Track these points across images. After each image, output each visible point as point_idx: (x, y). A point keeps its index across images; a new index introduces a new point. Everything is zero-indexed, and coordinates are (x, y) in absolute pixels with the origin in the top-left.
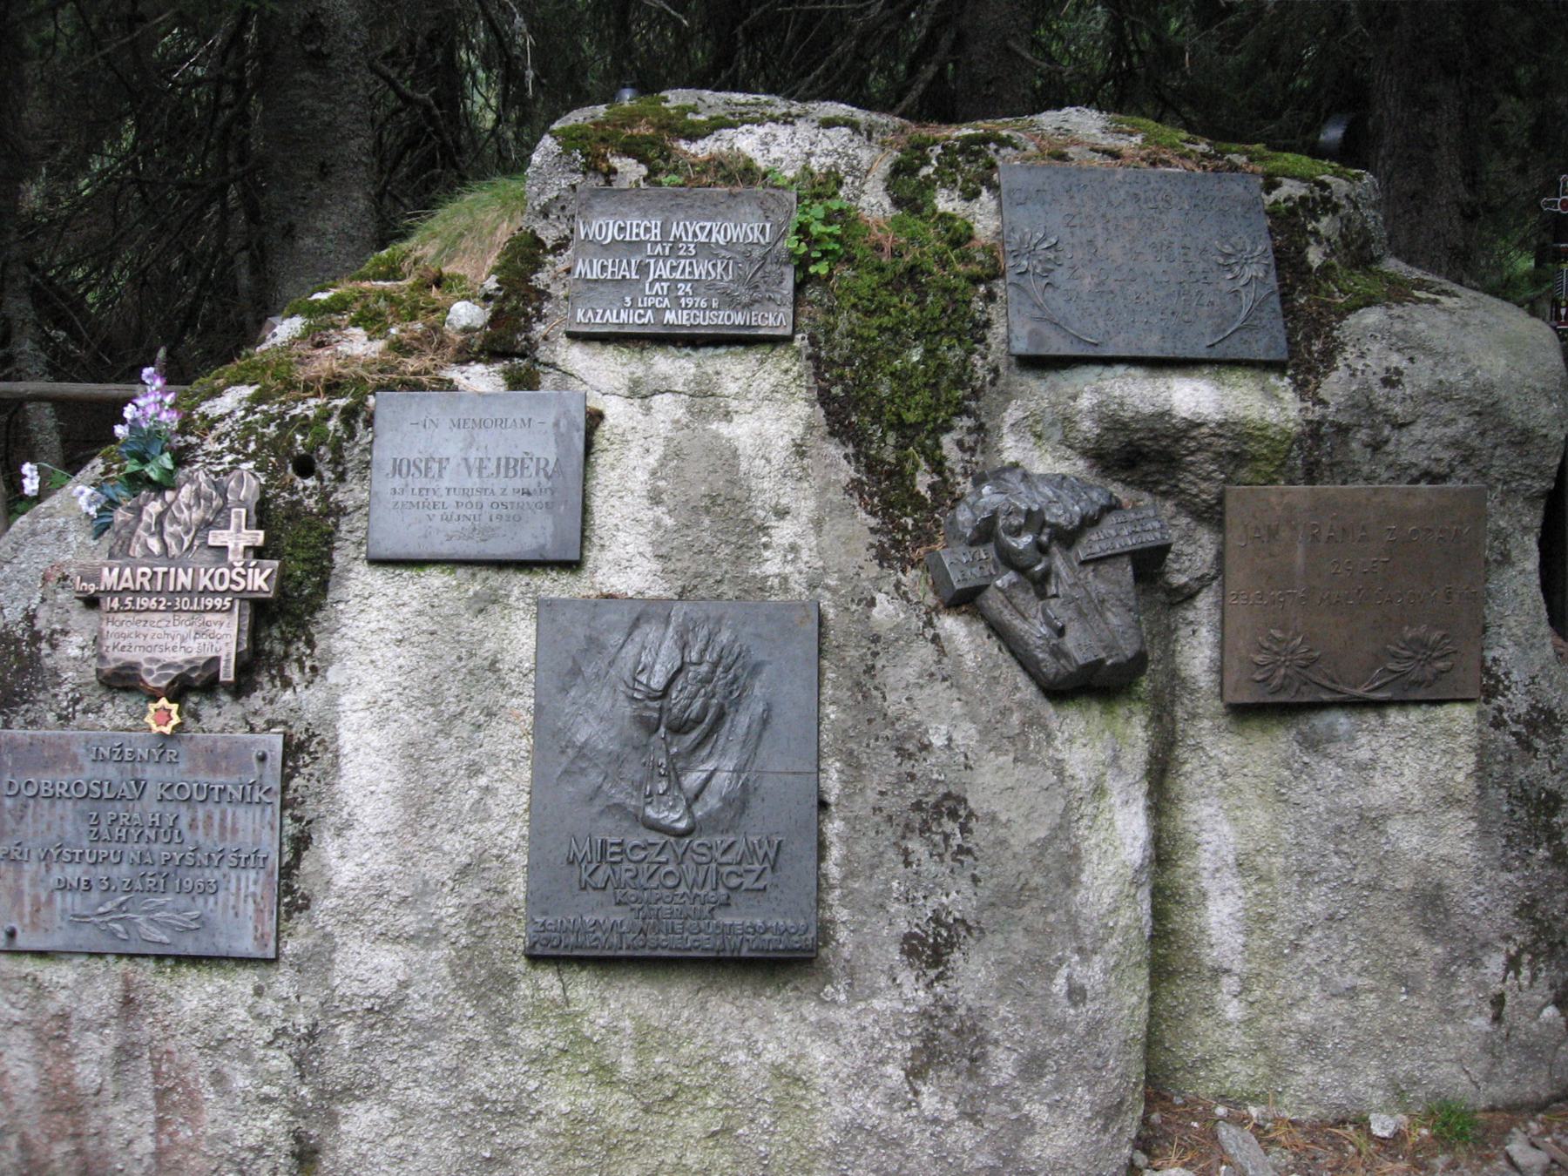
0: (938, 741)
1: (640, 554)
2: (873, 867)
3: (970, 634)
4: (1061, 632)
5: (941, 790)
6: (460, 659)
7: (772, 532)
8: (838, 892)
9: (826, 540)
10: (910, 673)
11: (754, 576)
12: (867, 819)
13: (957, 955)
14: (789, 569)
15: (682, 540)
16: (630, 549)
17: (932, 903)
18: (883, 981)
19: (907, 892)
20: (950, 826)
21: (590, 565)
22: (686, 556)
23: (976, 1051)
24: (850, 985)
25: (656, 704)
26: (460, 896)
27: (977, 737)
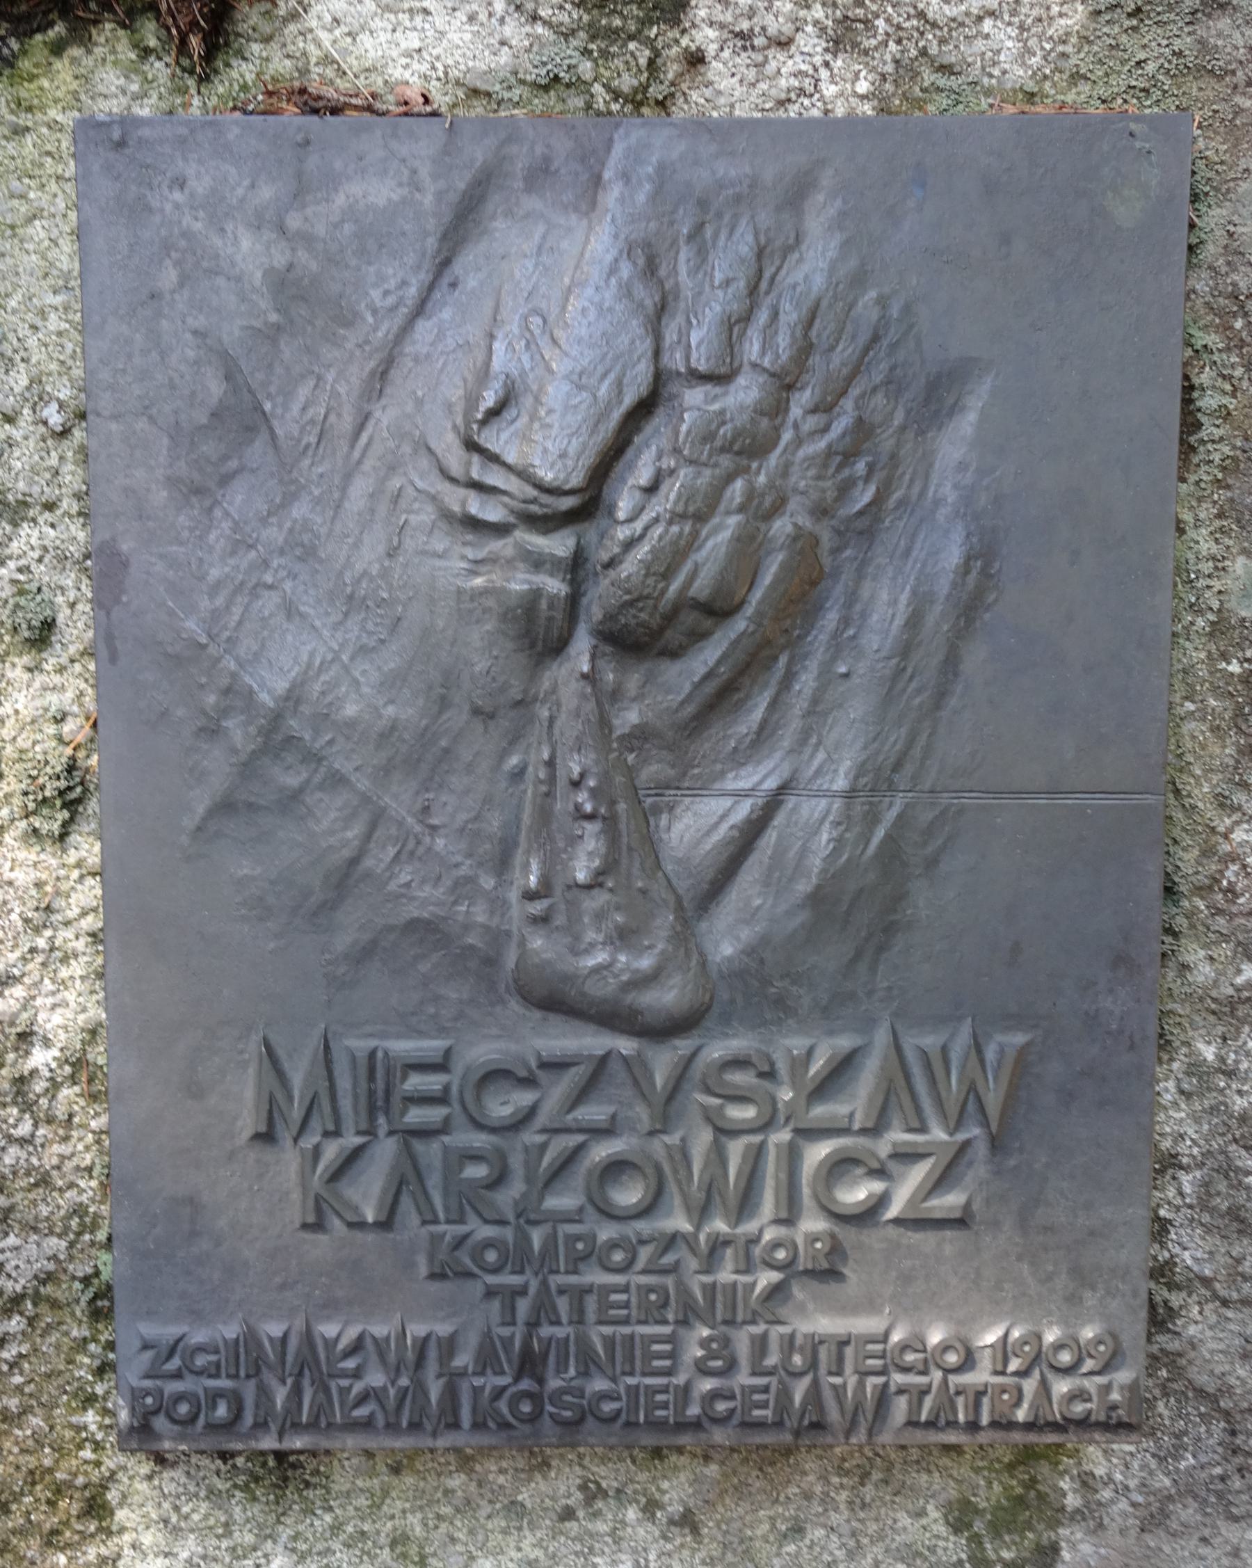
25: (559, 545)
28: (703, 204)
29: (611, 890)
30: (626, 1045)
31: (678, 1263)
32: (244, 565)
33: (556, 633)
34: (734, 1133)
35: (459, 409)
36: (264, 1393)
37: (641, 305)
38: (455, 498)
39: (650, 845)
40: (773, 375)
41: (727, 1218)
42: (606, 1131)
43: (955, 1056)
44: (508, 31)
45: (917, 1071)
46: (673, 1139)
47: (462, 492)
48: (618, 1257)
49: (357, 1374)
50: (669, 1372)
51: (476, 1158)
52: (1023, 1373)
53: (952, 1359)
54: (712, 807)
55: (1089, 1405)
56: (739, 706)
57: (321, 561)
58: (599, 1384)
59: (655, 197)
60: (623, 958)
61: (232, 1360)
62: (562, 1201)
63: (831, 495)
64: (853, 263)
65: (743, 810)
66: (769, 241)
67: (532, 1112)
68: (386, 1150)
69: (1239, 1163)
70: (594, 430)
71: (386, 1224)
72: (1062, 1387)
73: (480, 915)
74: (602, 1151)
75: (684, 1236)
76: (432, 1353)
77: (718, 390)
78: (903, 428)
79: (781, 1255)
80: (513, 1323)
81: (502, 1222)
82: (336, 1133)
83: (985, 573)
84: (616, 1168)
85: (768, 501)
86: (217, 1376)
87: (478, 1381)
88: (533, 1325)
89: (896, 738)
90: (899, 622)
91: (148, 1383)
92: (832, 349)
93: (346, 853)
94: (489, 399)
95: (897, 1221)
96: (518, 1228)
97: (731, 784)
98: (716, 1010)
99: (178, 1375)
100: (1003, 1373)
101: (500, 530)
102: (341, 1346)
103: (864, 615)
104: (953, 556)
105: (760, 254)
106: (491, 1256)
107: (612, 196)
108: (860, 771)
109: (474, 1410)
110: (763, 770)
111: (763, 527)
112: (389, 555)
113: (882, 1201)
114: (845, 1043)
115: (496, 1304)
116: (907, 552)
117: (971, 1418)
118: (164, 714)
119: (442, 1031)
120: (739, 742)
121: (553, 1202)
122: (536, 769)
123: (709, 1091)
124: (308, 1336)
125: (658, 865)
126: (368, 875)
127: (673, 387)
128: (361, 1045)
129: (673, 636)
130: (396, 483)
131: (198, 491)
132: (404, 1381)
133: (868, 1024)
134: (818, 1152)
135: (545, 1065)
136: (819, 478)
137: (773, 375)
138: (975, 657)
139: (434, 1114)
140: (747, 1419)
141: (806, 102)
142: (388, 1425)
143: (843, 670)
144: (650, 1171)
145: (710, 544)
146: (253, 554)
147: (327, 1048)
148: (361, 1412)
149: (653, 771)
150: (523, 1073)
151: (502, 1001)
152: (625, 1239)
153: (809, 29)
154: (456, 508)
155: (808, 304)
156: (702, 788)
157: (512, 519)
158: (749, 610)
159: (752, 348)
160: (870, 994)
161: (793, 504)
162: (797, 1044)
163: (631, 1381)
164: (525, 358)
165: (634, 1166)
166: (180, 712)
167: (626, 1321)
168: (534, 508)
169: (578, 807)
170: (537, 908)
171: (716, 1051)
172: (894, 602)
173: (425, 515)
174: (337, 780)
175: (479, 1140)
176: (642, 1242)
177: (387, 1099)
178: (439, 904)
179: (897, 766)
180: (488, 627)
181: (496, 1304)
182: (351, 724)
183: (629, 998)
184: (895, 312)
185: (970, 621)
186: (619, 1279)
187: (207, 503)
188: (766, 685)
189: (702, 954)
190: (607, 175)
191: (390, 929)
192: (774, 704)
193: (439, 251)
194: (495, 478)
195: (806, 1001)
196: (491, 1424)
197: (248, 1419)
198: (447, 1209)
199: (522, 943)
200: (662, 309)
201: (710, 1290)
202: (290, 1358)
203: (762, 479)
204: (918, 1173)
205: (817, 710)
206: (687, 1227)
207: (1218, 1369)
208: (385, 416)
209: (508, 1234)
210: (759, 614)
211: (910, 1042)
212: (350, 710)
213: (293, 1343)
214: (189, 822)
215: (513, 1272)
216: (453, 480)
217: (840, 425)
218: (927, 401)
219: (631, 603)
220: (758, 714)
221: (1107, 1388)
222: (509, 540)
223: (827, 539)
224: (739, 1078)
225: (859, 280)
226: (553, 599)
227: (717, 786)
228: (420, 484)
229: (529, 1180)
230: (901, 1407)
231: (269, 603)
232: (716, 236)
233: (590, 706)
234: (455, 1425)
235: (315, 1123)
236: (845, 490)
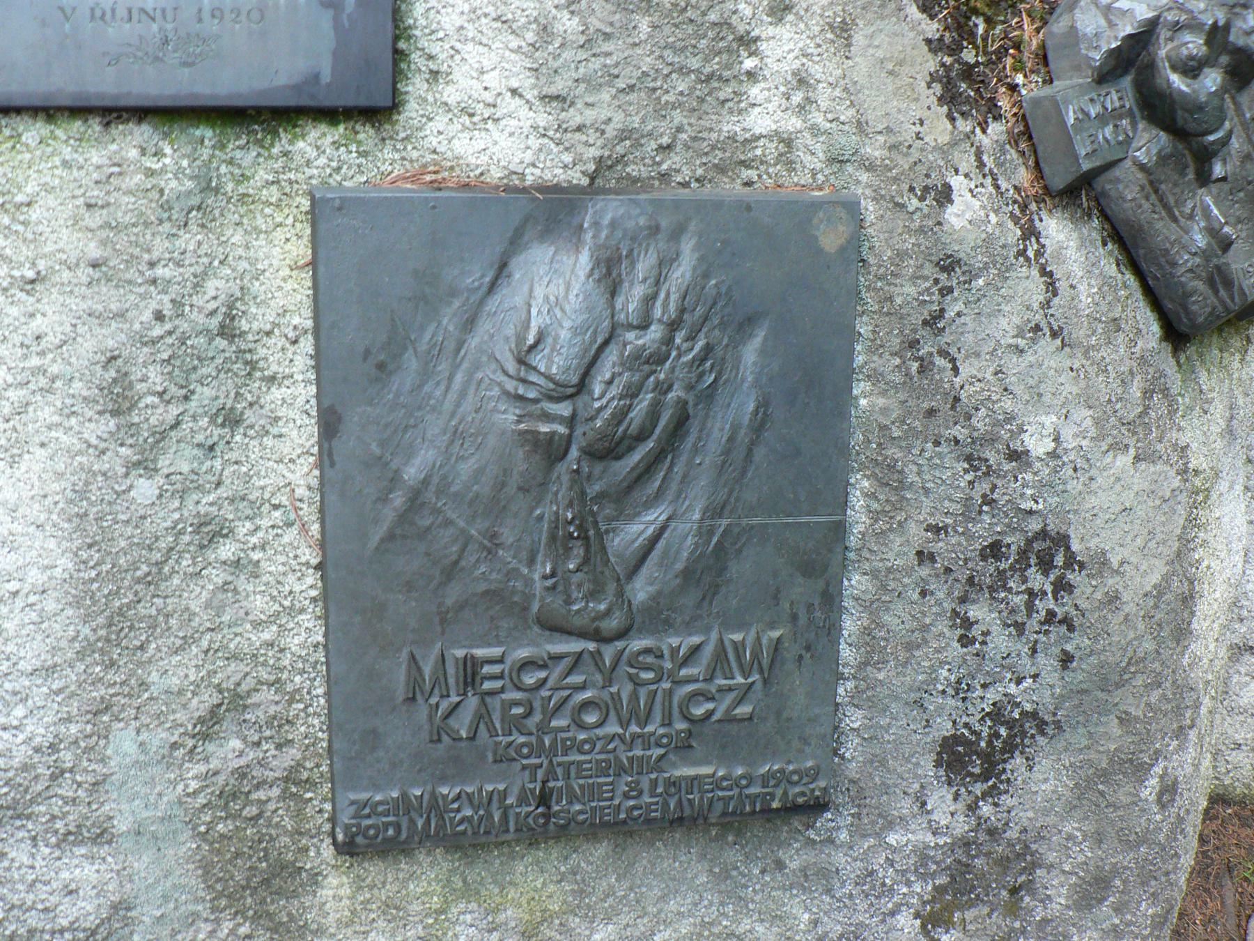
0: (1038, 445)
1: (514, 92)
2: (910, 647)
3: (1082, 243)
4: (1226, 245)
5: (1034, 525)
6: (159, 317)
7: (763, 46)
8: (850, 685)
9: (861, 67)
10: (1005, 326)
11: (732, 138)
12: (909, 571)
13: (1019, 760)
14: (793, 123)
15: (596, 64)
16: (492, 79)
17: (992, 695)
18: (905, 806)
19: (959, 682)
20: (1037, 580)
21: (412, 111)
22: (605, 96)
23: (1022, 879)
24: (858, 816)
25: (564, 409)
26: (206, 760)
27: (1093, 432)
30: (591, 646)
35: (513, 339)
36: (412, 822)
38: (510, 385)
41: (639, 724)
42: (583, 687)
44: (530, 142)
46: (614, 689)
47: (515, 383)
48: (587, 747)
49: (458, 810)
51: (517, 703)
52: (776, 786)
53: (744, 782)
54: (635, 528)
58: (578, 807)
60: (591, 605)
63: (693, 380)
65: (650, 530)
67: (545, 680)
68: (472, 702)
71: (472, 738)
75: (619, 736)
76: (495, 798)
78: (727, 346)
79: (665, 741)
81: (531, 734)
84: (586, 705)
85: (665, 386)
86: (388, 815)
87: (518, 810)
88: (544, 782)
90: (725, 439)
91: (353, 821)
93: (454, 558)
94: (531, 340)
95: (719, 721)
96: (538, 736)
98: (636, 626)
99: (369, 816)
102: (450, 797)
103: (708, 436)
104: (751, 407)
106: (525, 751)
107: (588, 236)
108: (705, 511)
109: (516, 823)
110: (659, 511)
113: (710, 713)
114: (696, 640)
115: (527, 772)
116: (729, 405)
119: (499, 644)
121: (554, 723)
123: (632, 666)
124: (433, 794)
126: (462, 569)
127: (619, 331)
128: (460, 653)
130: (479, 375)
132: (481, 812)
133: (708, 629)
138: (760, 453)
139: (498, 684)
142: (474, 833)
144: (603, 706)
147: (443, 655)
148: (461, 828)
150: (541, 663)
151: (530, 627)
152: (591, 738)
154: (512, 390)
155: (684, 288)
156: (631, 519)
158: (655, 437)
159: (658, 312)
162: (674, 641)
163: (593, 804)
164: (547, 318)
165: (597, 704)
167: (591, 777)
168: (554, 394)
170: (549, 583)
172: (722, 429)
173: (496, 392)
174: (448, 523)
175: (518, 695)
177: (473, 680)
178: (501, 582)
181: (527, 772)
184: (724, 290)
186: (588, 757)
189: (629, 601)
190: (586, 225)
191: (474, 595)
194: (533, 378)
195: (679, 620)
198: (503, 729)
201: (631, 760)
202: (425, 805)
204: (729, 699)
206: (621, 731)
208: (473, 342)
209: (533, 739)
210: (659, 438)
213: (426, 797)
216: (509, 376)
217: (700, 344)
220: (657, 484)
221: (813, 790)
223: (691, 399)
224: (650, 659)
226: (561, 436)
228: (491, 376)
229: (543, 713)
230: (719, 807)
232: (639, 255)
234: (507, 831)
235: (436, 691)
236: (701, 376)
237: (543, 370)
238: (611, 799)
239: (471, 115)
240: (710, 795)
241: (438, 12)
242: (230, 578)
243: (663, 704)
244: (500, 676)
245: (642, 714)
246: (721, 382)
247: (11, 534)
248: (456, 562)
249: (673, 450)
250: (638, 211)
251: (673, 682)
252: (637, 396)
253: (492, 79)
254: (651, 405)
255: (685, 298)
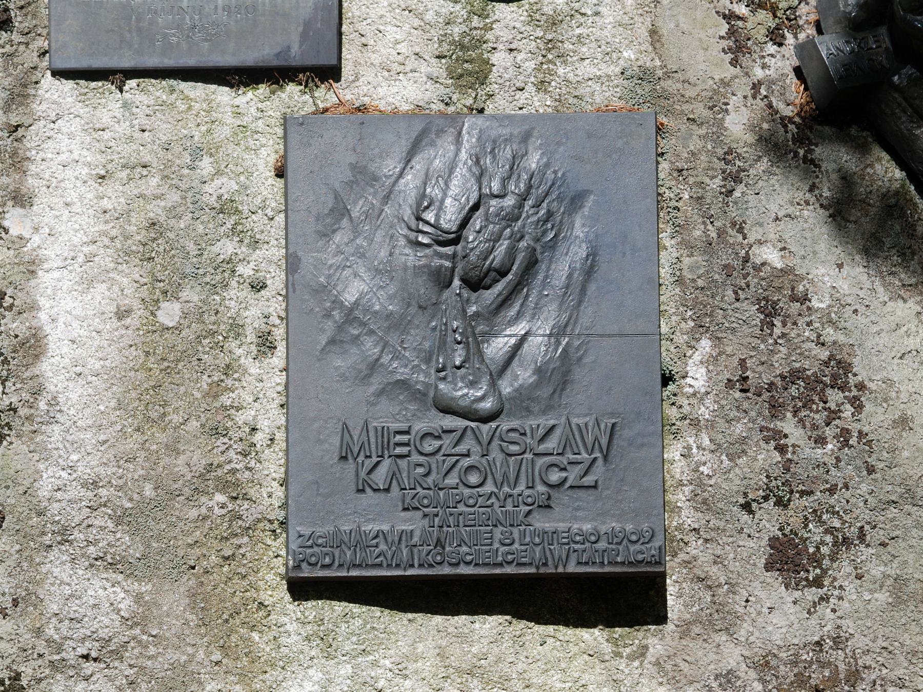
25: (449, 250)
28: (494, 142)
29: (467, 368)
31: (493, 503)
32: (340, 259)
33: (448, 280)
34: (510, 455)
35: (414, 206)
37: (474, 173)
38: (412, 235)
39: (480, 353)
40: (519, 195)
41: (509, 486)
43: (591, 424)
45: (576, 433)
47: (415, 234)
50: (491, 545)
53: (593, 538)
55: (644, 556)
56: (511, 305)
57: (366, 258)
59: (479, 139)
61: (332, 540)
62: (452, 480)
64: (545, 160)
65: (513, 341)
66: (517, 153)
69: (705, 482)
70: (460, 213)
72: (632, 548)
73: (422, 378)
74: (466, 462)
77: (501, 200)
78: (564, 213)
80: (433, 527)
81: (429, 489)
82: (370, 457)
83: (593, 260)
84: (471, 468)
85: (518, 236)
89: (564, 317)
92: (539, 187)
93: (375, 357)
97: (508, 332)
98: (505, 412)
99: (311, 547)
100: (612, 543)
101: (427, 246)
105: (514, 157)
111: (517, 244)
112: (390, 255)
117: (601, 561)
118: (312, 310)
120: (511, 318)
122: (441, 326)
125: (484, 361)
126: (382, 365)
129: (488, 281)
131: (325, 235)
134: (541, 462)
135: (444, 432)
136: (535, 229)
137: (519, 195)
140: (519, 562)
141: (530, 108)
142: (388, 565)
143: (546, 293)
145: (499, 249)
146: (342, 256)
149: (480, 328)
153: (530, 84)
157: (433, 242)
158: (512, 272)
160: (559, 406)
161: (527, 237)
162: (532, 423)
166: (317, 309)
167: (475, 526)
169: (455, 339)
171: (505, 426)
173: (402, 242)
175: (421, 459)
176: (480, 496)
179: (566, 326)
180: (424, 278)
182: (376, 312)
183: (475, 406)
184: (559, 175)
185: (589, 276)
187: (328, 239)
188: (519, 299)
191: (389, 384)
192: (522, 305)
193: (407, 157)
196: (426, 566)
197: (337, 564)
199: (436, 387)
200: (481, 175)
203: (516, 229)
205: (538, 308)
207: (706, 569)
211: (574, 421)
212: (377, 308)
214: (319, 348)
215: (433, 508)
218: (571, 204)
219: (473, 269)
222: (431, 249)
225: (547, 165)
227: (504, 333)
231: (347, 272)
232: (499, 152)
233: (459, 305)
235: (362, 453)
236: (545, 232)
237: (432, 221)
238: (491, 545)
239: (389, 71)
240: (567, 547)
241: (368, 8)
242: (223, 377)
243: (527, 471)
244: (407, 444)
245: (512, 477)
246: (561, 237)
247: (80, 336)
248: (377, 360)
249: (528, 284)
250: (497, 124)
251: (534, 454)
252: (499, 241)
253: (402, 48)
254: (508, 248)
255: (531, 179)
